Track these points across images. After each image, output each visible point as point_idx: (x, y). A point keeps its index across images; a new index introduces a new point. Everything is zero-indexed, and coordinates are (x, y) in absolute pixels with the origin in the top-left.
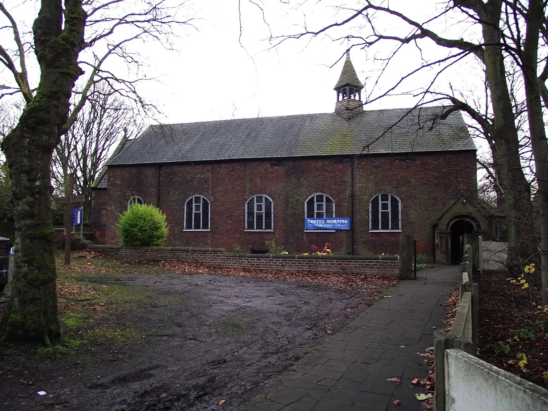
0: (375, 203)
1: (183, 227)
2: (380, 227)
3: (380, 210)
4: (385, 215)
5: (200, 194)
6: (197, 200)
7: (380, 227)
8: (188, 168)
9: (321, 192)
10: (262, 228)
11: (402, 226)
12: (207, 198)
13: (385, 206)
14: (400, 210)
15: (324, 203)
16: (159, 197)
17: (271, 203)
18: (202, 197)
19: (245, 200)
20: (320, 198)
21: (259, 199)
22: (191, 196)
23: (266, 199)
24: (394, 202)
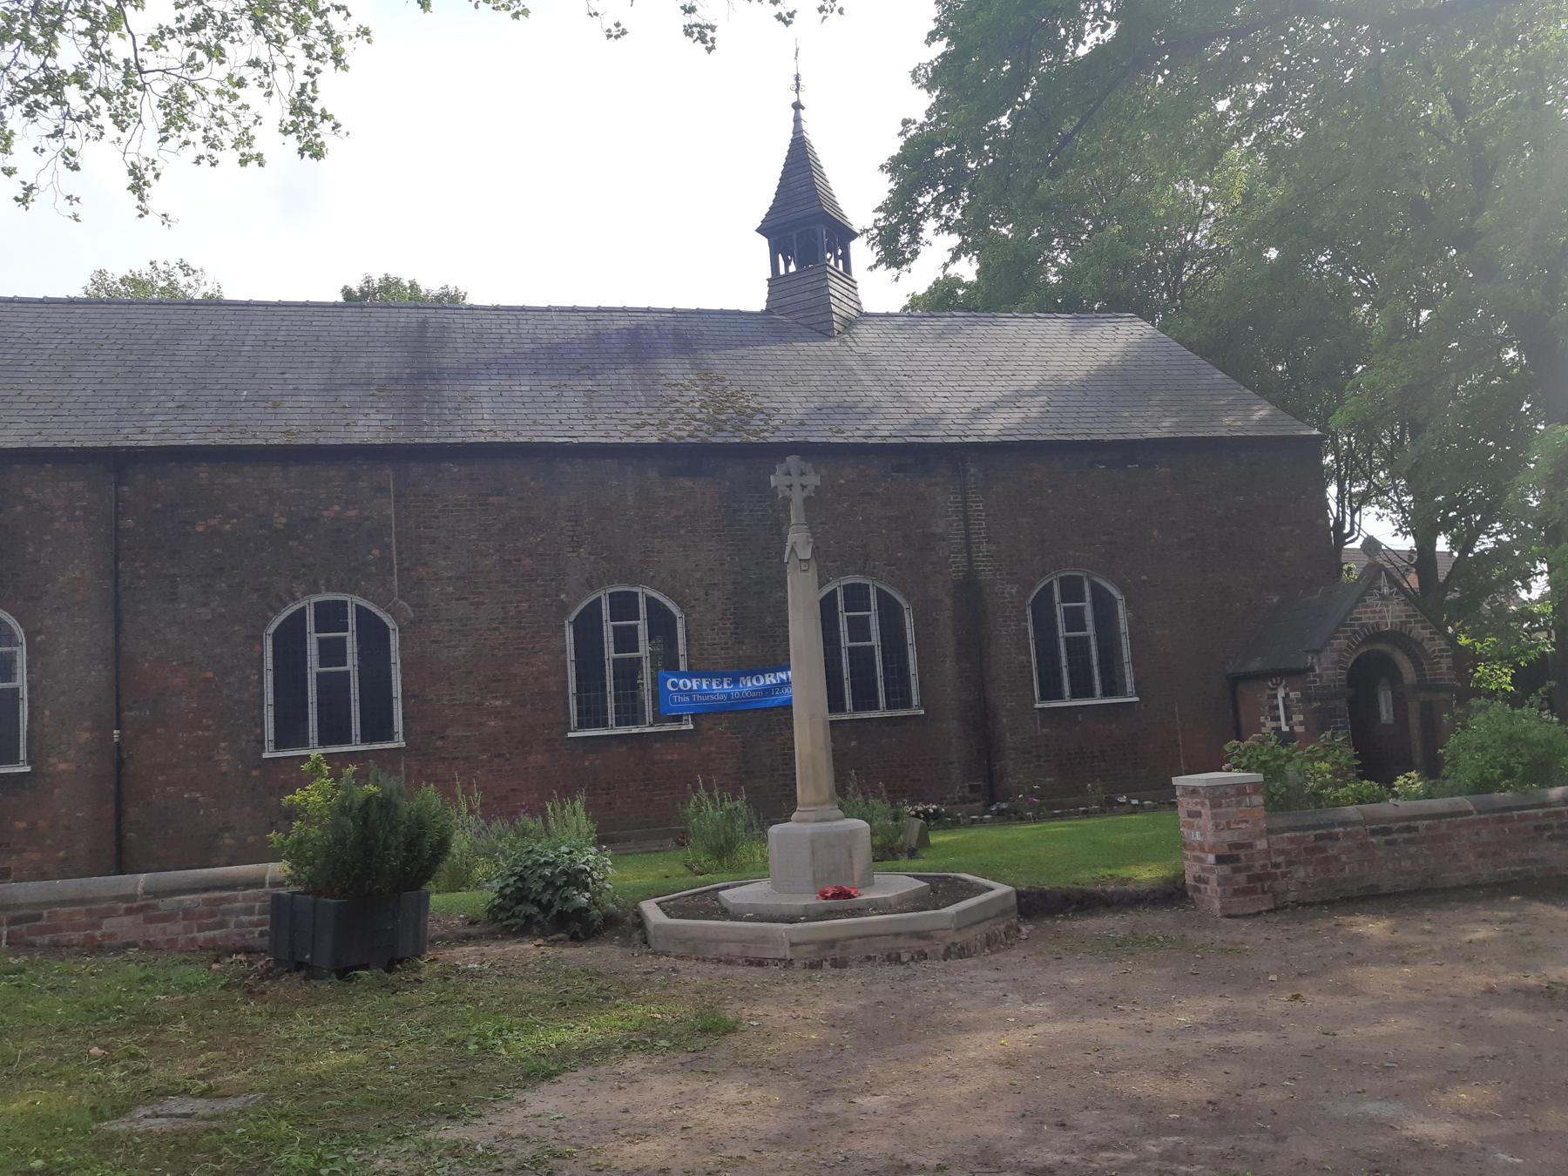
0: (588, 626)
1: (260, 741)
2: (1098, 691)
3: (610, 653)
4: (333, 689)
5: (342, 590)
6: (624, 606)
7: (1098, 691)
8: (203, 473)
9: (861, 572)
10: (843, 710)
11: (1137, 684)
12: (380, 605)
13: (1074, 619)
14: (1124, 627)
15: (351, 639)
16: (117, 610)
17: (1114, 601)
18: (353, 601)
19: (564, 609)
20: (1072, 589)
21: (1072, 589)
22: (295, 599)
23: (651, 602)
24: (890, 612)
